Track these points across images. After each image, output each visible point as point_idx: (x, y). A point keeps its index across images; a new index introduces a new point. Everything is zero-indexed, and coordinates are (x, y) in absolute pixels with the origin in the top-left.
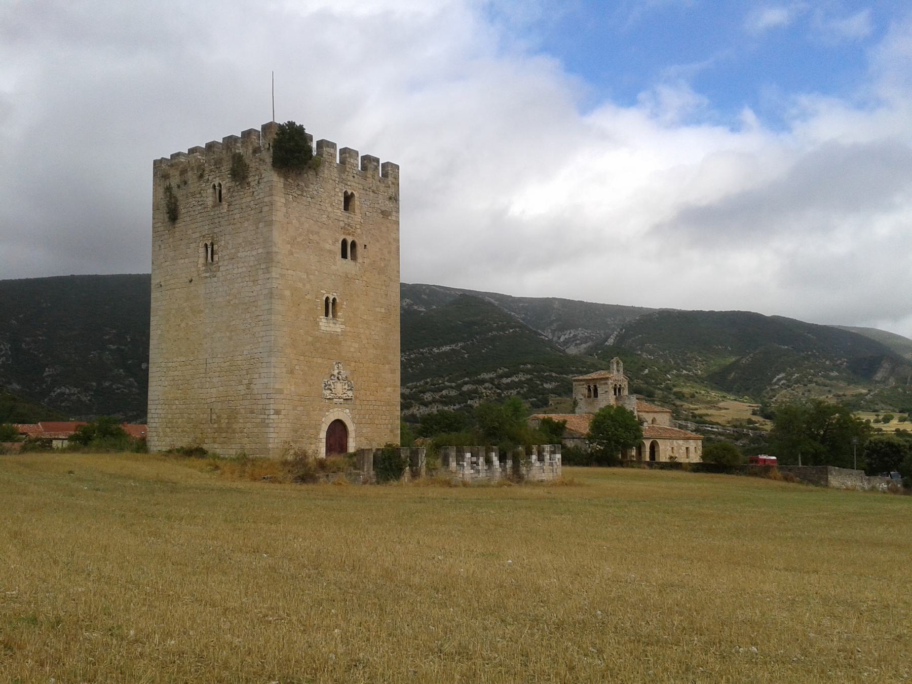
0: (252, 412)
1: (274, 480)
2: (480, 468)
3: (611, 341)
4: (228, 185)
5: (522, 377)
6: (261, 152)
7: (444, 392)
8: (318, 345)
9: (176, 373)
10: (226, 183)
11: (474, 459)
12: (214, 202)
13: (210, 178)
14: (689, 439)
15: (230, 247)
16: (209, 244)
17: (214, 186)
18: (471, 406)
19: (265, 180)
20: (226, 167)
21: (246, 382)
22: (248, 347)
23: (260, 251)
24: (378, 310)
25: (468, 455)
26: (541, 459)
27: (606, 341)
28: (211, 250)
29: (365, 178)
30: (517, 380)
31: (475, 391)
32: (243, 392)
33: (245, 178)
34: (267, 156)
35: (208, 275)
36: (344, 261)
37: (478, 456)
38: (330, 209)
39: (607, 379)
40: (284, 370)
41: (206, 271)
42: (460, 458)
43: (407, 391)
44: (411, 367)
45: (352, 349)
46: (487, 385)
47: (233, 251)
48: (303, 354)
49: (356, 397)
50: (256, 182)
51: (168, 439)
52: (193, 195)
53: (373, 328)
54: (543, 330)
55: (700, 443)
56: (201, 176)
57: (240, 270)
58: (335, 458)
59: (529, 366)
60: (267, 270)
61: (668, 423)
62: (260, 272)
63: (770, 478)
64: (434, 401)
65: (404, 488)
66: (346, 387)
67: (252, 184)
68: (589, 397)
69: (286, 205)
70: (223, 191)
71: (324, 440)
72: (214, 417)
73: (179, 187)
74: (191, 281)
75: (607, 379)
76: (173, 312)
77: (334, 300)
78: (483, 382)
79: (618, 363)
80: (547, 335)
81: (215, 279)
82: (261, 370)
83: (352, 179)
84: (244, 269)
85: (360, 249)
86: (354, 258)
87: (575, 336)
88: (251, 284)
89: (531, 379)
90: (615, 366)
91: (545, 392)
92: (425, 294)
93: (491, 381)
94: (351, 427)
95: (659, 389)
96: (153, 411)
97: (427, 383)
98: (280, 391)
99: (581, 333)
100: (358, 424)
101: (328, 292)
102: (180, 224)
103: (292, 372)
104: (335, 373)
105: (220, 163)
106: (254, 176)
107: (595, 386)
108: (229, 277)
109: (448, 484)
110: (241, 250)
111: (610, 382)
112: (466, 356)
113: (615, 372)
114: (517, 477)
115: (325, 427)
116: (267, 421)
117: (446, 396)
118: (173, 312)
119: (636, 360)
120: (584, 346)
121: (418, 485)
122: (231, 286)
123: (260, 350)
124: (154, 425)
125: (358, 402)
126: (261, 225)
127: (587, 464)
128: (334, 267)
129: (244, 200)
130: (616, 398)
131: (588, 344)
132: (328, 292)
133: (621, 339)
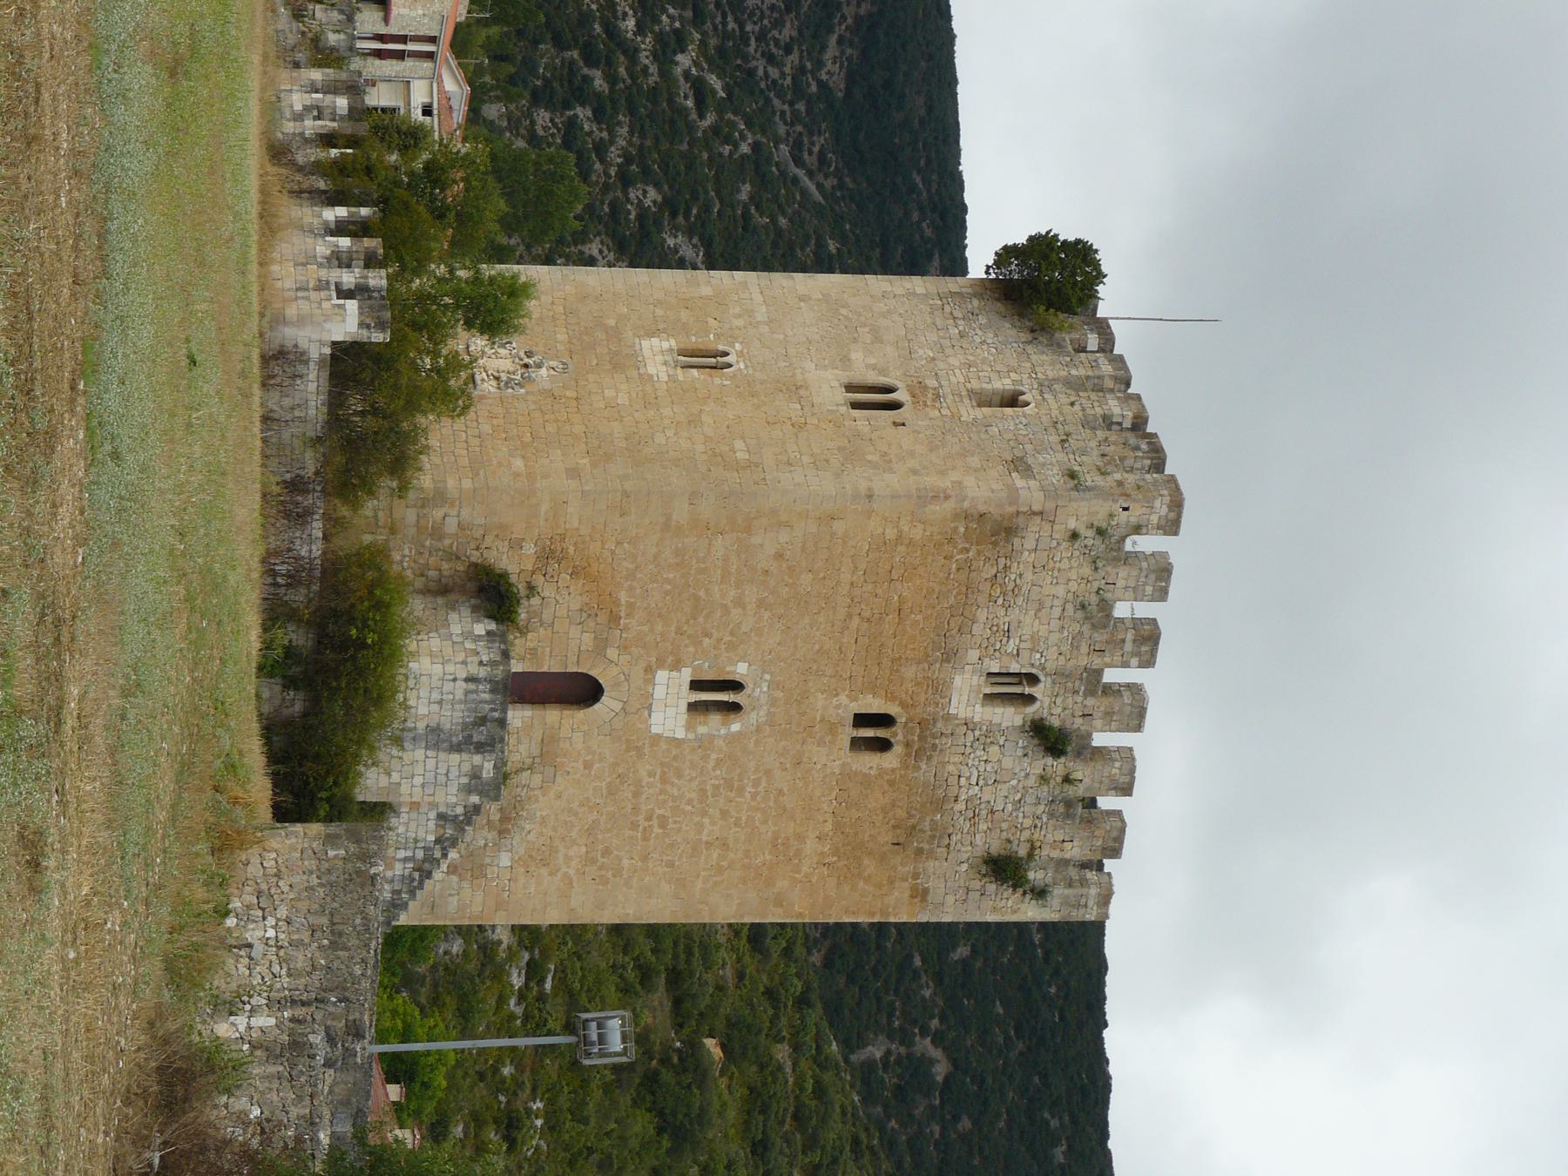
101: (740, 354)
132: (740, 354)
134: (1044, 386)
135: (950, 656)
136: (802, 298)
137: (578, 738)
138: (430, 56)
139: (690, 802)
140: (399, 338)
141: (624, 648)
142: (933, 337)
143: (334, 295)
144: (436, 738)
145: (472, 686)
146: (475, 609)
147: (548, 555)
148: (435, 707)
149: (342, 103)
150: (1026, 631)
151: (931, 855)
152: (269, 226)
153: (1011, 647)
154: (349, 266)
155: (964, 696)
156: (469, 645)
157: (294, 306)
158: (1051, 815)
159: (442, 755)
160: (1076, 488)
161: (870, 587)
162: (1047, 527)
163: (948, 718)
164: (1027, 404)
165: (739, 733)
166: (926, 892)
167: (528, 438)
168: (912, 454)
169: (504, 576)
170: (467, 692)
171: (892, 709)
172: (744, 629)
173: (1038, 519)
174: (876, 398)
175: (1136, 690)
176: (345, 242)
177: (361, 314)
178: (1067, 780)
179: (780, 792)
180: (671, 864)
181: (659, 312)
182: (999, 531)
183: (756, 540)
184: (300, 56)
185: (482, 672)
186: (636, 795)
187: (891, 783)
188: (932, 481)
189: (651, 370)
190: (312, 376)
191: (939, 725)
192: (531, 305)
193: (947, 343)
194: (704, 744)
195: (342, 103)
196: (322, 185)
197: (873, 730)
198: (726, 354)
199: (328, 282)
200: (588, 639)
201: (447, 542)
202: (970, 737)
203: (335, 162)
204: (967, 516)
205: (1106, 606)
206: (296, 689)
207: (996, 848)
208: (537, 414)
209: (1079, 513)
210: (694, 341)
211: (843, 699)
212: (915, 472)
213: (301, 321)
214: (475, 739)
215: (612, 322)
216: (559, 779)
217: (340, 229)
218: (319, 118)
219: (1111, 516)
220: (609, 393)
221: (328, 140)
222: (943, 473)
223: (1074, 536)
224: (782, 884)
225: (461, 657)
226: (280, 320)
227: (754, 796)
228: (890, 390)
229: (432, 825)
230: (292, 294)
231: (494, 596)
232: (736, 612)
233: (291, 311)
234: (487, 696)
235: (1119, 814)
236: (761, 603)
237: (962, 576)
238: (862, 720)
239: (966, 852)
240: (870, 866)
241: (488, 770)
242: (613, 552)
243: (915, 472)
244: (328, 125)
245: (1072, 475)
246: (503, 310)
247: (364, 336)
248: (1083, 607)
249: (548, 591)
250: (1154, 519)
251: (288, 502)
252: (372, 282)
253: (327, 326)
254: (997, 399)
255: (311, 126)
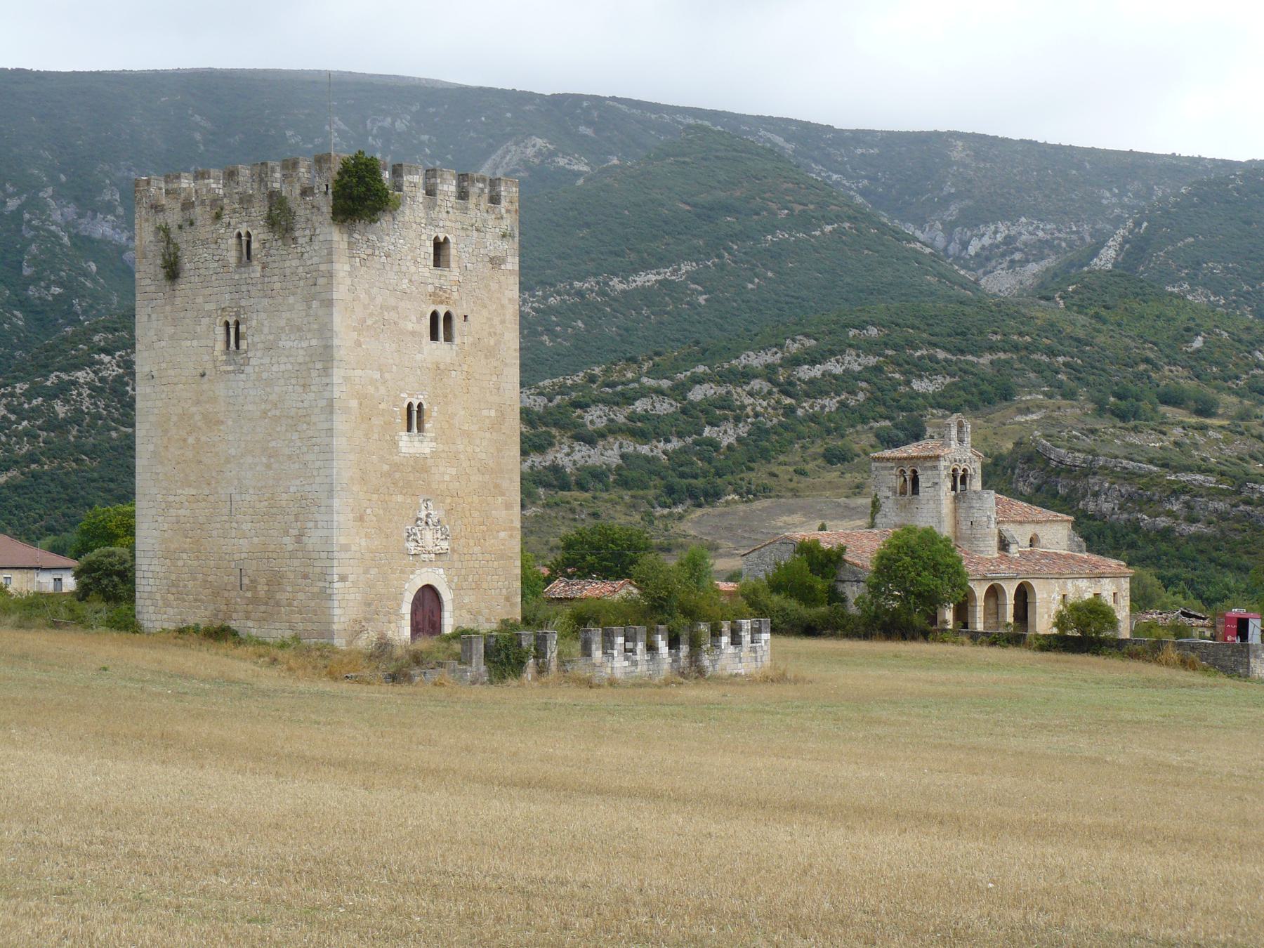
0: (305, 577)
1: (359, 680)
2: (638, 658)
3: (1107, 257)
4: (262, 236)
5: (853, 362)
6: (313, 195)
7: (640, 406)
8: (397, 475)
9: (182, 512)
10: (259, 234)
11: (630, 645)
12: (240, 259)
13: (233, 222)
14: (1101, 576)
15: (266, 330)
16: (231, 322)
17: (239, 235)
18: (713, 444)
19: (321, 238)
20: (259, 210)
21: (295, 532)
22: (298, 482)
23: (314, 342)
24: (485, 413)
25: (620, 640)
26: (736, 640)
27: (1095, 253)
28: (234, 333)
29: (465, 210)
30: (838, 370)
31: (724, 403)
32: (290, 548)
33: (289, 229)
34: (326, 207)
35: (230, 368)
36: (434, 344)
37: (634, 641)
38: (413, 269)
39: (937, 458)
40: (351, 516)
41: (227, 363)
42: (608, 645)
43: (539, 404)
44: (550, 331)
45: (447, 478)
46: (756, 384)
47: (271, 337)
48: (376, 491)
49: (453, 550)
50: (307, 239)
51: (171, 611)
52: (205, 243)
53: (478, 442)
54: (920, 223)
55: (1125, 584)
56: (218, 217)
57: (283, 367)
58: (424, 644)
59: (873, 331)
60: (326, 371)
61: (1065, 542)
62: (314, 374)
63: (1159, 662)
64: (612, 430)
65: (525, 691)
66: (439, 535)
67: (300, 241)
68: (903, 493)
69: (350, 274)
70: (254, 245)
71: (408, 617)
72: (246, 581)
73: (180, 227)
74: (203, 375)
75: (937, 458)
76: (174, 418)
77: (420, 405)
78: (745, 376)
79: (960, 426)
80: (927, 237)
81: (243, 376)
82: (318, 517)
83: (444, 215)
84: (289, 367)
85: (457, 323)
86: (449, 338)
87: (1009, 240)
88: (300, 389)
89: (878, 369)
90: (954, 433)
91: (912, 404)
92: (590, 124)
93: (769, 372)
94: (447, 596)
95: (1231, 391)
96: (144, 568)
97: (592, 379)
98: (345, 548)
99: (1027, 230)
100: (457, 590)
101: (410, 395)
102: (183, 286)
103: (361, 518)
104: (423, 515)
105: (249, 201)
106: (304, 229)
107: (915, 472)
108: (265, 375)
109: (589, 684)
110: (283, 336)
111: (943, 464)
112: (702, 299)
113: (954, 444)
114: (695, 670)
115: (409, 598)
116: (329, 591)
117: (645, 417)
118: (174, 418)
119: (1170, 312)
120: (1033, 268)
121: (546, 685)
122: (268, 389)
123: (315, 487)
124: (148, 589)
125: (456, 557)
126: (315, 304)
127: (866, 636)
128: (419, 357)
129: (288, 264)
130: (956, 498)
131: (1045, 263)
132: (410, 395)
133: (1136, 250)
189: (427, 451)
212: (503, 322)
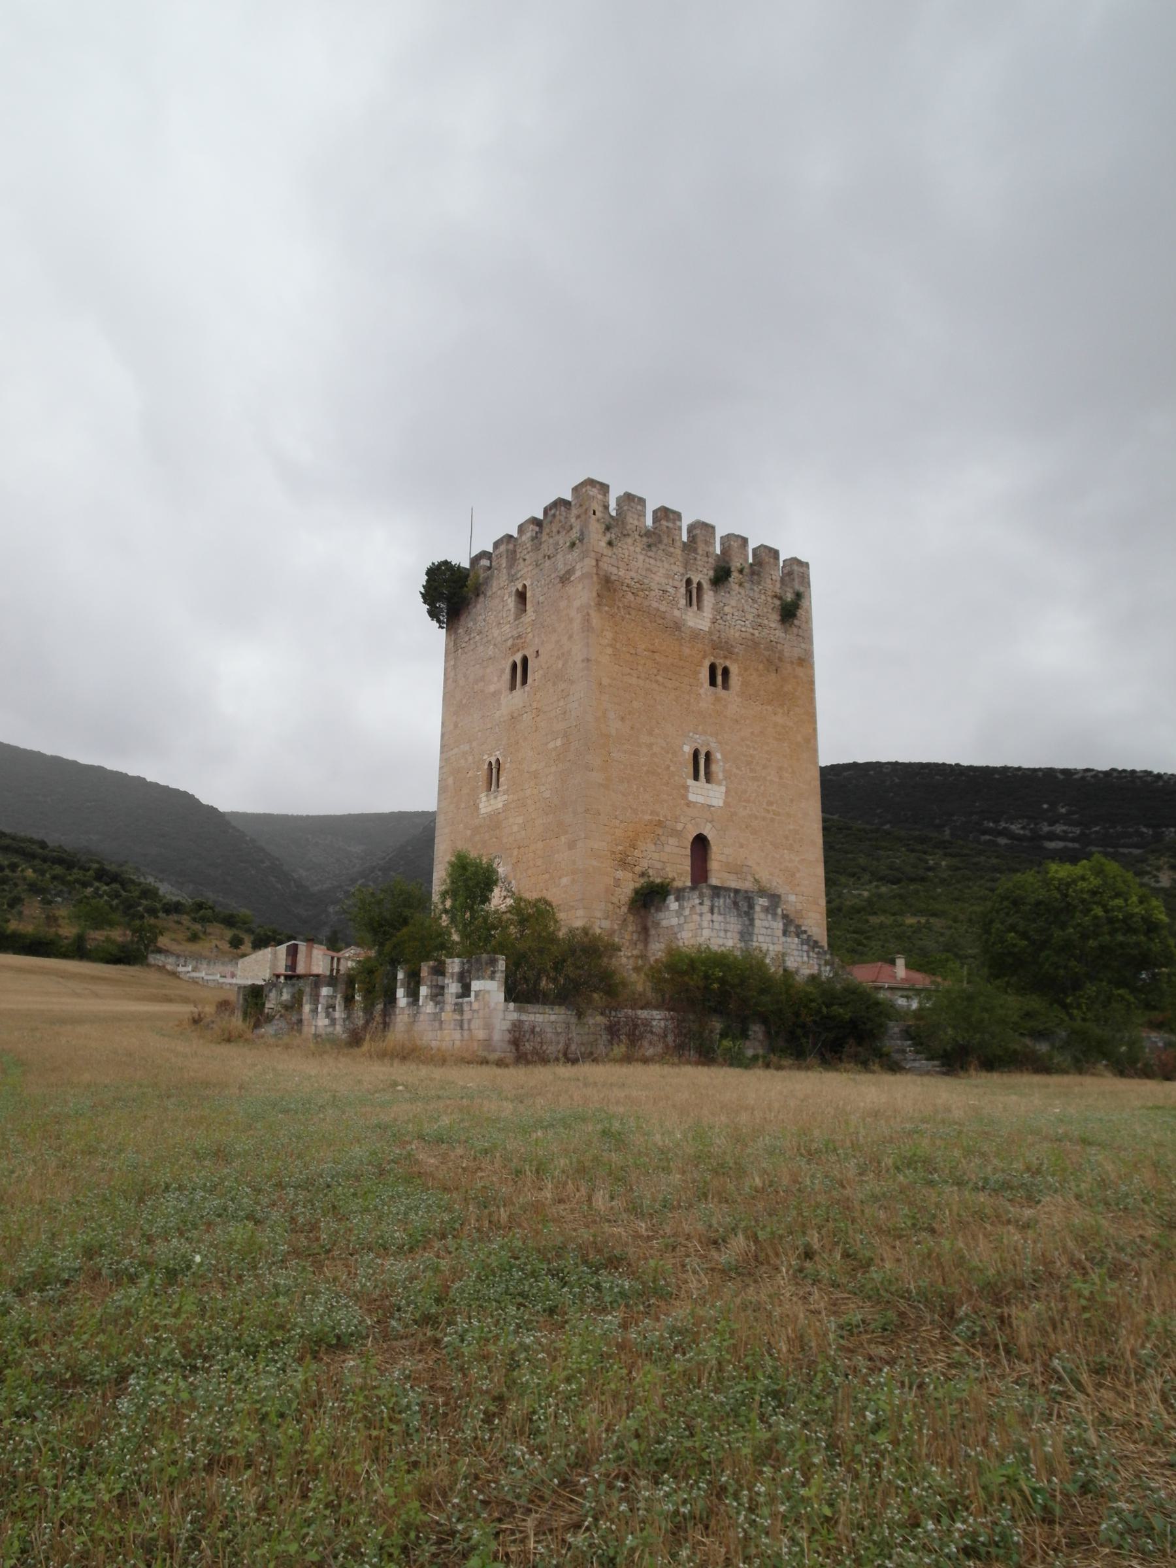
101: (490, 755)
132: (490, 755)
134: (512, 578)
135: (677, 626)
136: (456, 726)
137: (727, 851)
138: (339, 959)
139: (759, 787)
140: (501, 948)
141: (677, 819)
142: (481, 649)
143: (466, 999)
144: (746, 935)
145: (716, 910)
146: (659, 909)
147: (624, 863)
148: (729, 934)
149: (325, 991)
150: (664, 581)
151: (781, 652)
152: (409, 1054)
153: (671, 590)
154: (443, 988)
155: (699, 621)
156: (687, 912)
157: (475, 1032)
158: (759, 583)
159: (756, 931)
160: (581, 540)
161: (640, 668)
162: (605, 559)
163: (710, 633)
164: (525, 586)
165: (722, 755)
166: (799, 658)
167: (546, 876)
168: (558, 642)
169: (637, 892)
170: (720, 914)
171: (707, 664)
172: (664, 745)
173: (601, 563)
174: (520, 672)
175: (691, 528)
176: (424, 991)
177: (483, 978)
178: (741, 571)
179: (752, 733)
180: (792, 801)
181: (463, 805)
182: (608, 586)
183: (614, 732)
184: (294, 1019)
185: (707, 902)
186: (756, 818)
187: (746, 670)
188: (576, 625)
189: (500, 805)
190: (531, 1017)
191: (715, 638)
192: (473, 854)
193: (485, 640)
194: (728, 776)
195: (325, 991)
196: (380, 1007)
197: (718, 676)
198: (490, 763)
199: (456, 1004)
200: (672, 841)
201: (616, 927)
202: (720, 621)
203: (365, 998)
204: (599, 604)
205: (648, 534)
206: (747, 1030)
207: (775, 617)
208: (530, 872)
209: (597, 539)
210: (482, 783)
211: (702, 691)
212: (570, 637)
213: (488, 1026)
214: (746, 909)
215: (469, 832)
216: (749, 863)
217: (413, 994)
218: (334, 1008)
219: (598, 520)
220: (515, 828)
221: (349, 1000)
222: (571, 620)
223: (610, 544)
224: (799, 738)
225: (696, 917)
226: (487, 1043)
227: (755, 749)
228: (514, 666)
229: (789, 940)
230: (466, 1033)
231: (650, 897)
232: (656, 749)
233: (481, 1034)
234: (722, 901)
235: (754, 550)
236: (650, 733)
237: (633, 612)
238: (713, 682)
239: (779, 634)
240: (788, 688)
241: (762, 902)
242: (621, 822)
243: (570, 637)
244: (339, 1002)
245: (573, 545)
246: (476, 873)
247: (500, 976)
248: (649, 546)
249: (644, 864)
250: (600, 497)
251: (626, 1041)
252: (457, 969)
253: (492, 1005)
254: (520, 606)
255: (339, 1014)
